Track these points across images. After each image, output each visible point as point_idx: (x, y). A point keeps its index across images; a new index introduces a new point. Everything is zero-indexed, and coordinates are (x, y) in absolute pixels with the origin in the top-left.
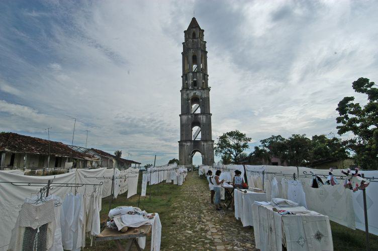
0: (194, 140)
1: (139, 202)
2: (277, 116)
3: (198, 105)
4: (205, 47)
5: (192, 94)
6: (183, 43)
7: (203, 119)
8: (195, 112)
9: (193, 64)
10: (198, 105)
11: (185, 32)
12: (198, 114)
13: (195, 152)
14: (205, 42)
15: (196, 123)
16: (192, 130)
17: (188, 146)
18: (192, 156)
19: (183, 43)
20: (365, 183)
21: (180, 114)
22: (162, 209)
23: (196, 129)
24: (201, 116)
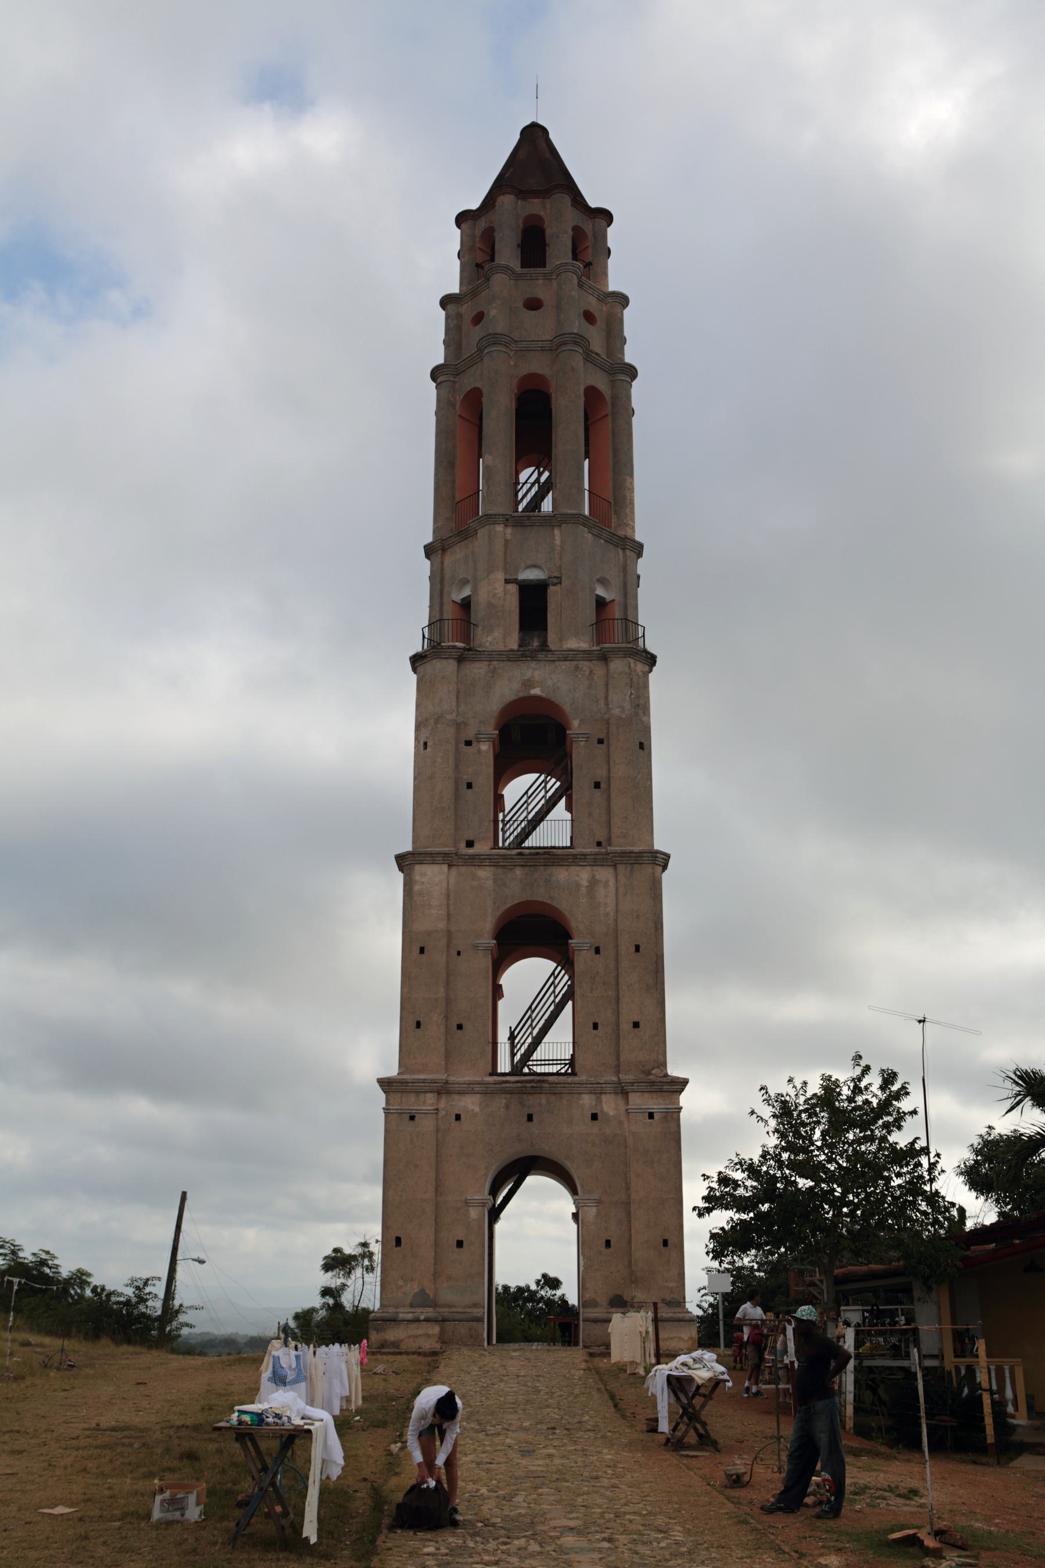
0: (516, 1070)
1: (63, 1350)
2: (647, 1332)
3: (553, 784)
4: (615, 336)
5: (507, 686)
6: (446, 302)
7: (586, 899)
8: (526, 834)
9: (522, 459)
10: (553, 784)
11: (463, 219)
12: (549, 856)
13: (513, 1173)
14: (622, 300)
15: (530, 930)
16: (497, 992)
17: (459, 1123)
18: (495, 1214)
19: (446, 302)
20: (459, 1517)
21: (406, 846)
22: (516, 514)
23: (528, 977)
24: (583, 875)
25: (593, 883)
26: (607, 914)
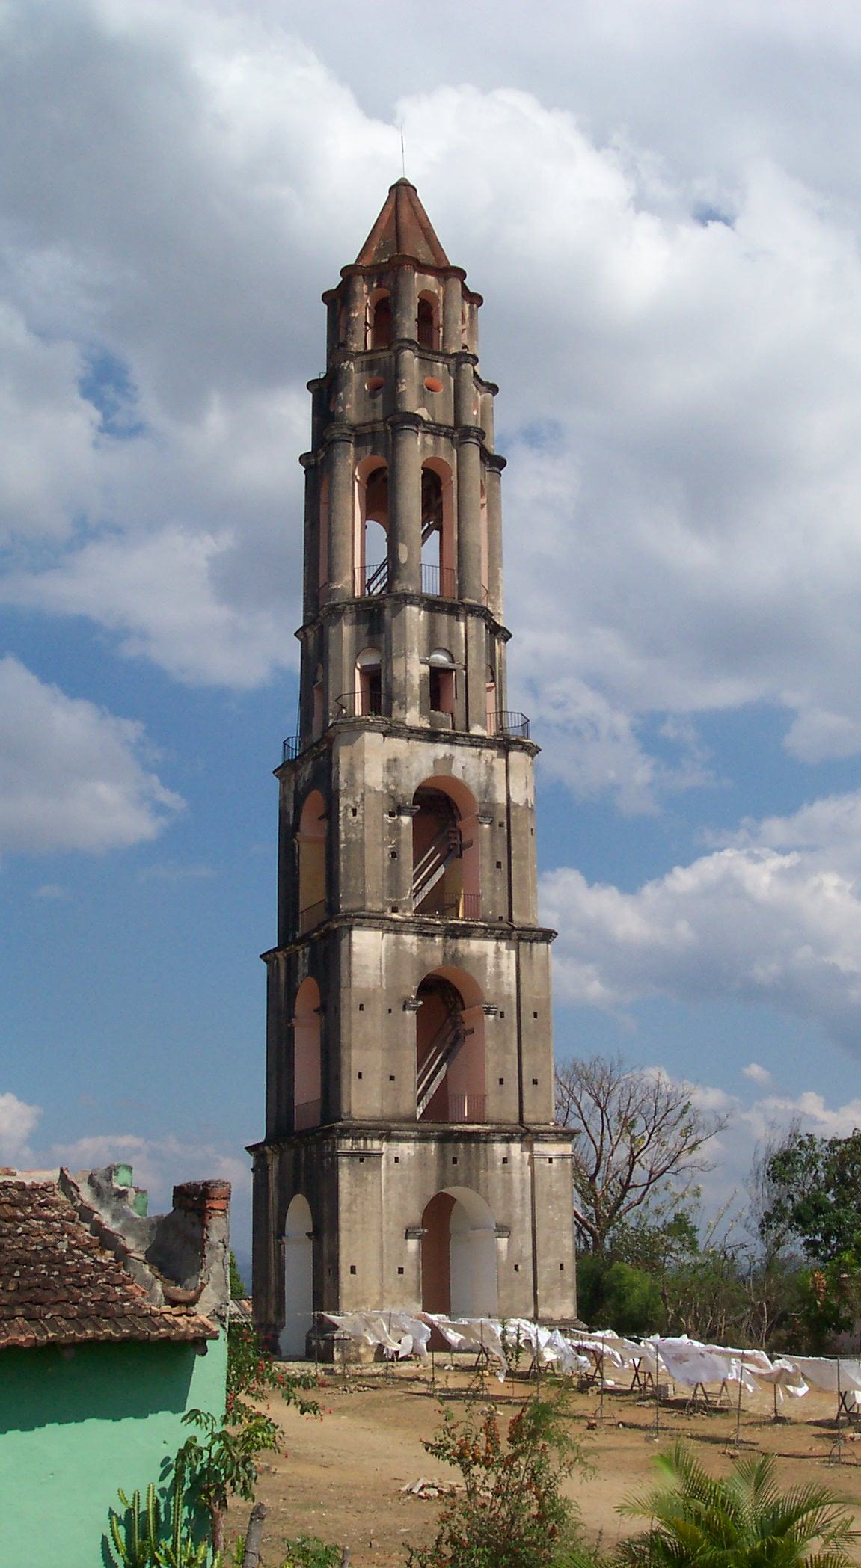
25: (498, 951)
26: (509, 984)
